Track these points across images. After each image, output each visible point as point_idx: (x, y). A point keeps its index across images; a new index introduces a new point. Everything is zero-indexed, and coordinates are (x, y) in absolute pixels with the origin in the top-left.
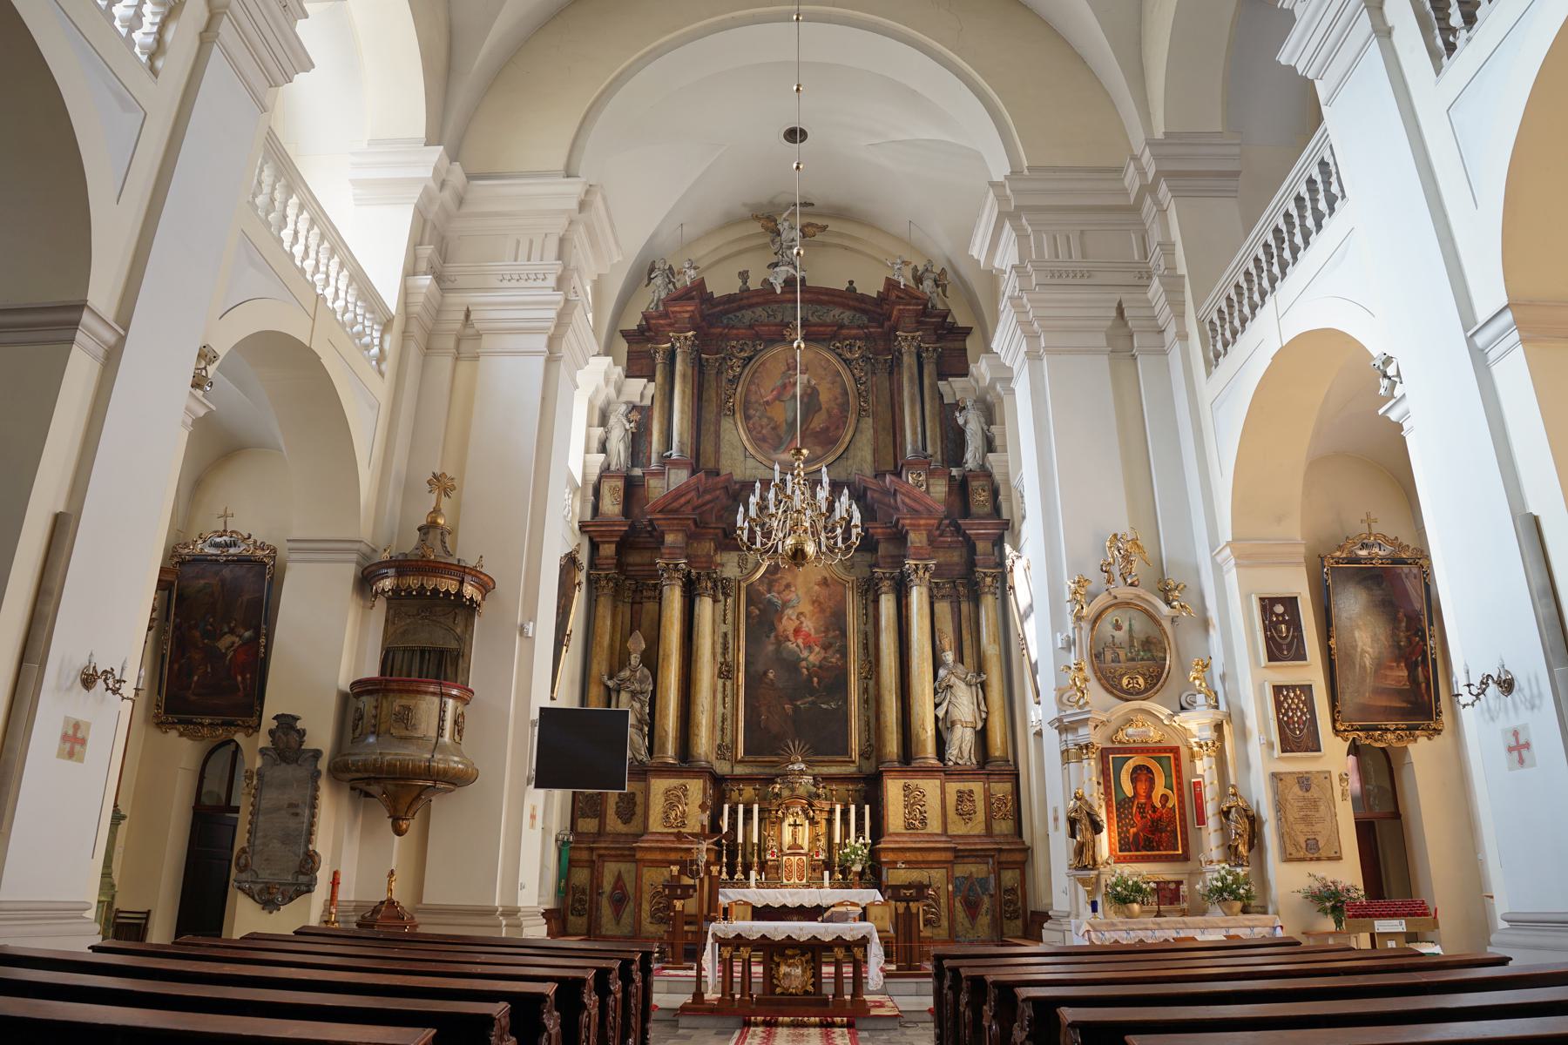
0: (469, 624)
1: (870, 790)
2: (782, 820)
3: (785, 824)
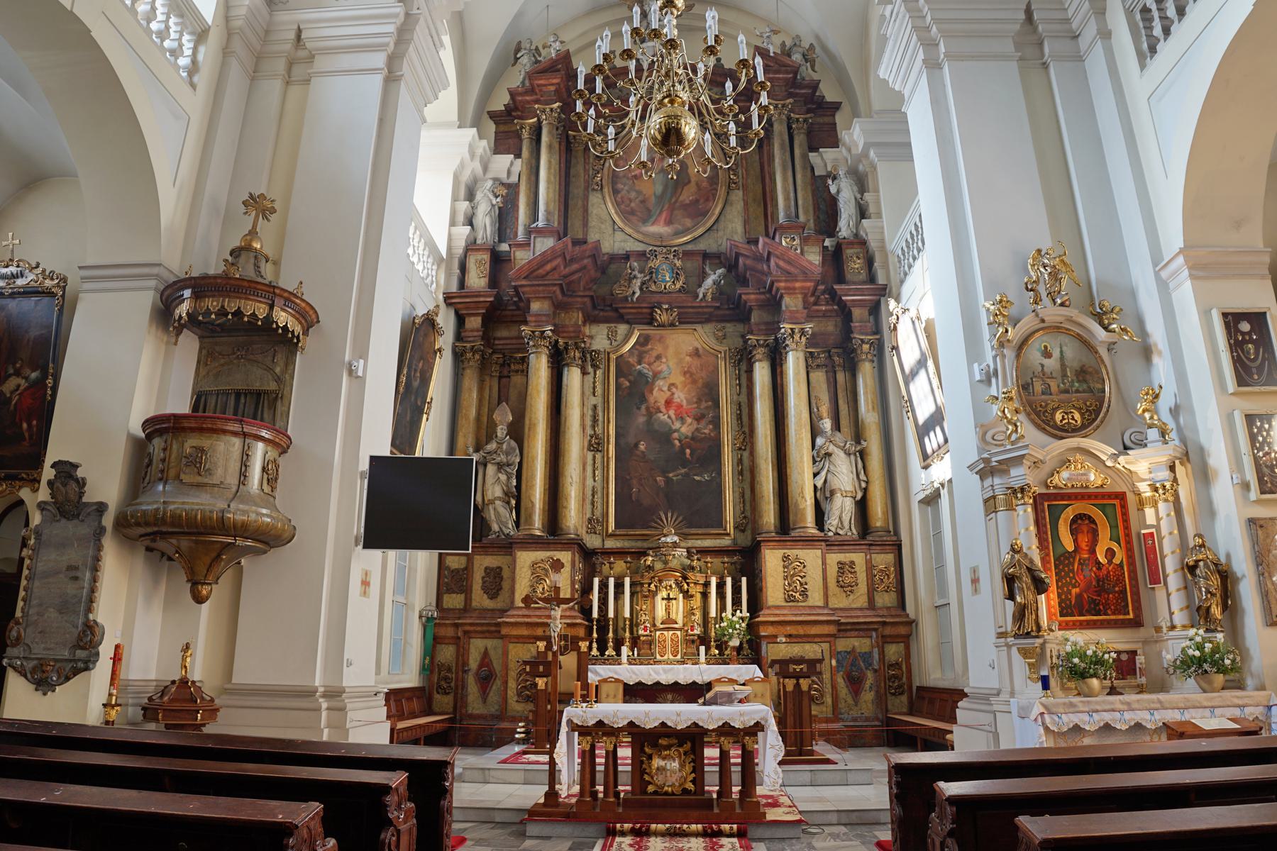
0: (290, 362)
1: (747, 562)
2: (655, 594)
3: (659, 598)
